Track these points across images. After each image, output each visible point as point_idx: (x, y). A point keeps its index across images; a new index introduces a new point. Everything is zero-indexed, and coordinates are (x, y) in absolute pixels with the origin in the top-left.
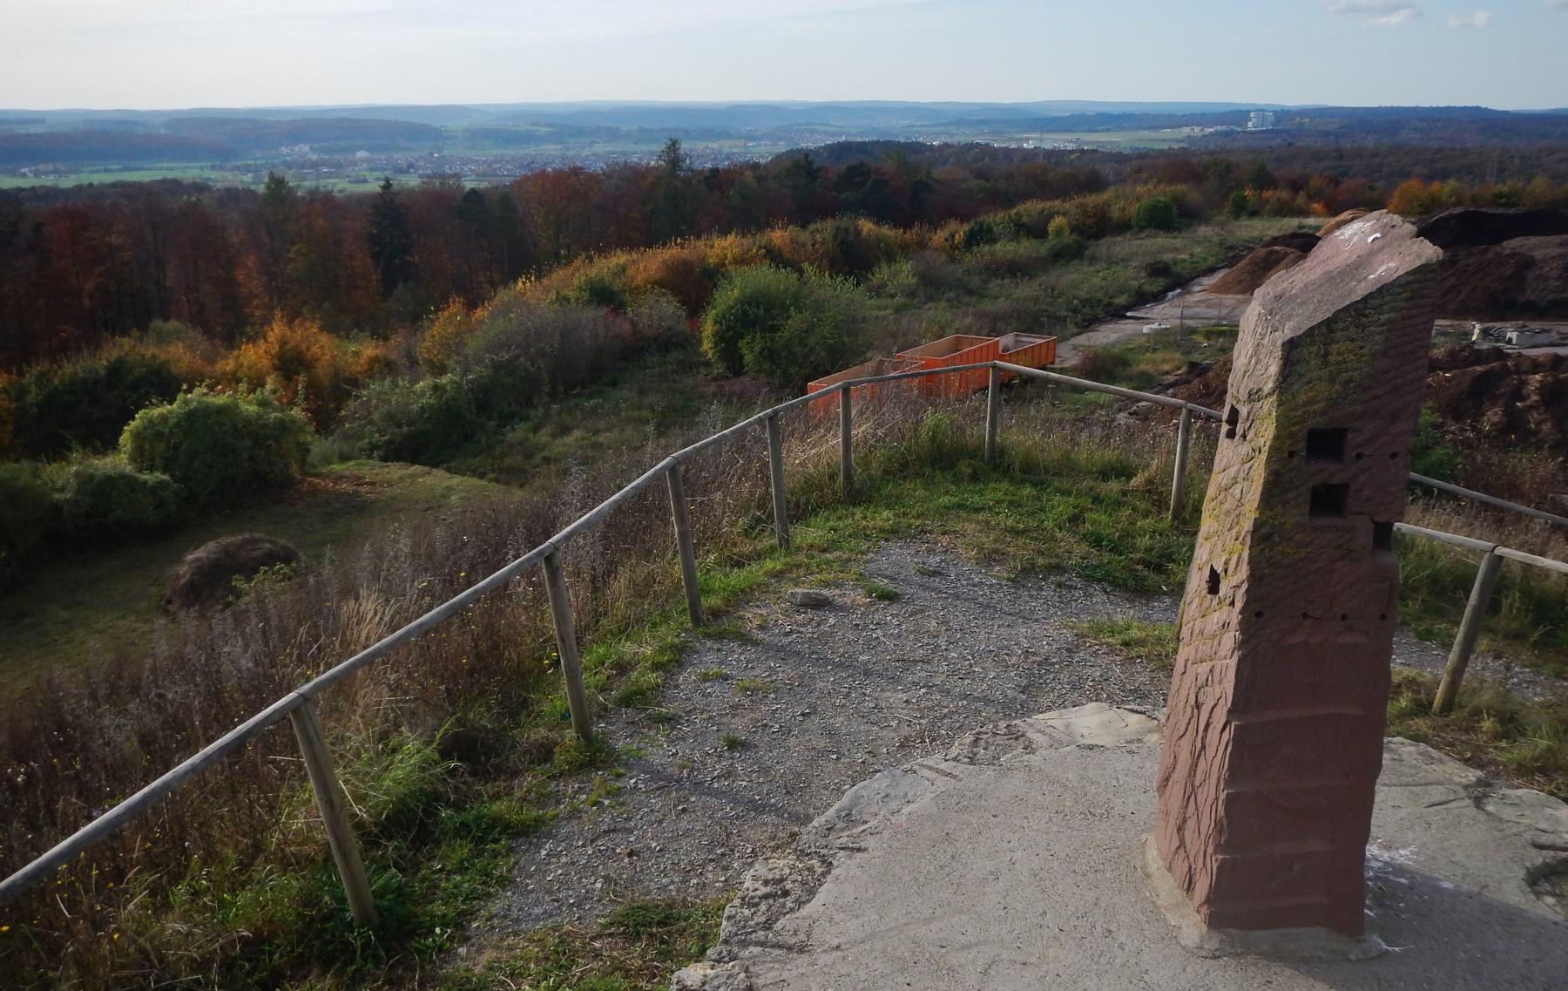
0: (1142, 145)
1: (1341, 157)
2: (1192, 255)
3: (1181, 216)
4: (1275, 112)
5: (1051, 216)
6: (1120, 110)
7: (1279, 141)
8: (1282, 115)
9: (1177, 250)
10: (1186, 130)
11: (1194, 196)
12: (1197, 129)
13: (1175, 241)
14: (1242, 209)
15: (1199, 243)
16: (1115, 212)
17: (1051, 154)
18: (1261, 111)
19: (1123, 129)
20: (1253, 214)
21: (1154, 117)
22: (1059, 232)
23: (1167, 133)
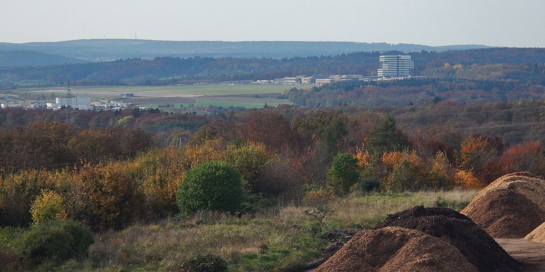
0: (226, 104)
1: (509, 118)
2: (264, 248)
3: (256, 189)
4: (413, 55)
5: (36, 192)
6: (193, 52)
7: (422, 96)
8: (424, 57)
9: (243, 240)
10: (289, 82)
11: (281, 163)
12: (305, 80)
13: (246, 228)
14: (350, 179)
15: (281, 229)
16: (148, 188)
17: (86, 117)
18: (394, 53)
19: (198, 80)
20: (371, 187)
21: (243, 62)
22: (50, 215)
23: (262, 86)
